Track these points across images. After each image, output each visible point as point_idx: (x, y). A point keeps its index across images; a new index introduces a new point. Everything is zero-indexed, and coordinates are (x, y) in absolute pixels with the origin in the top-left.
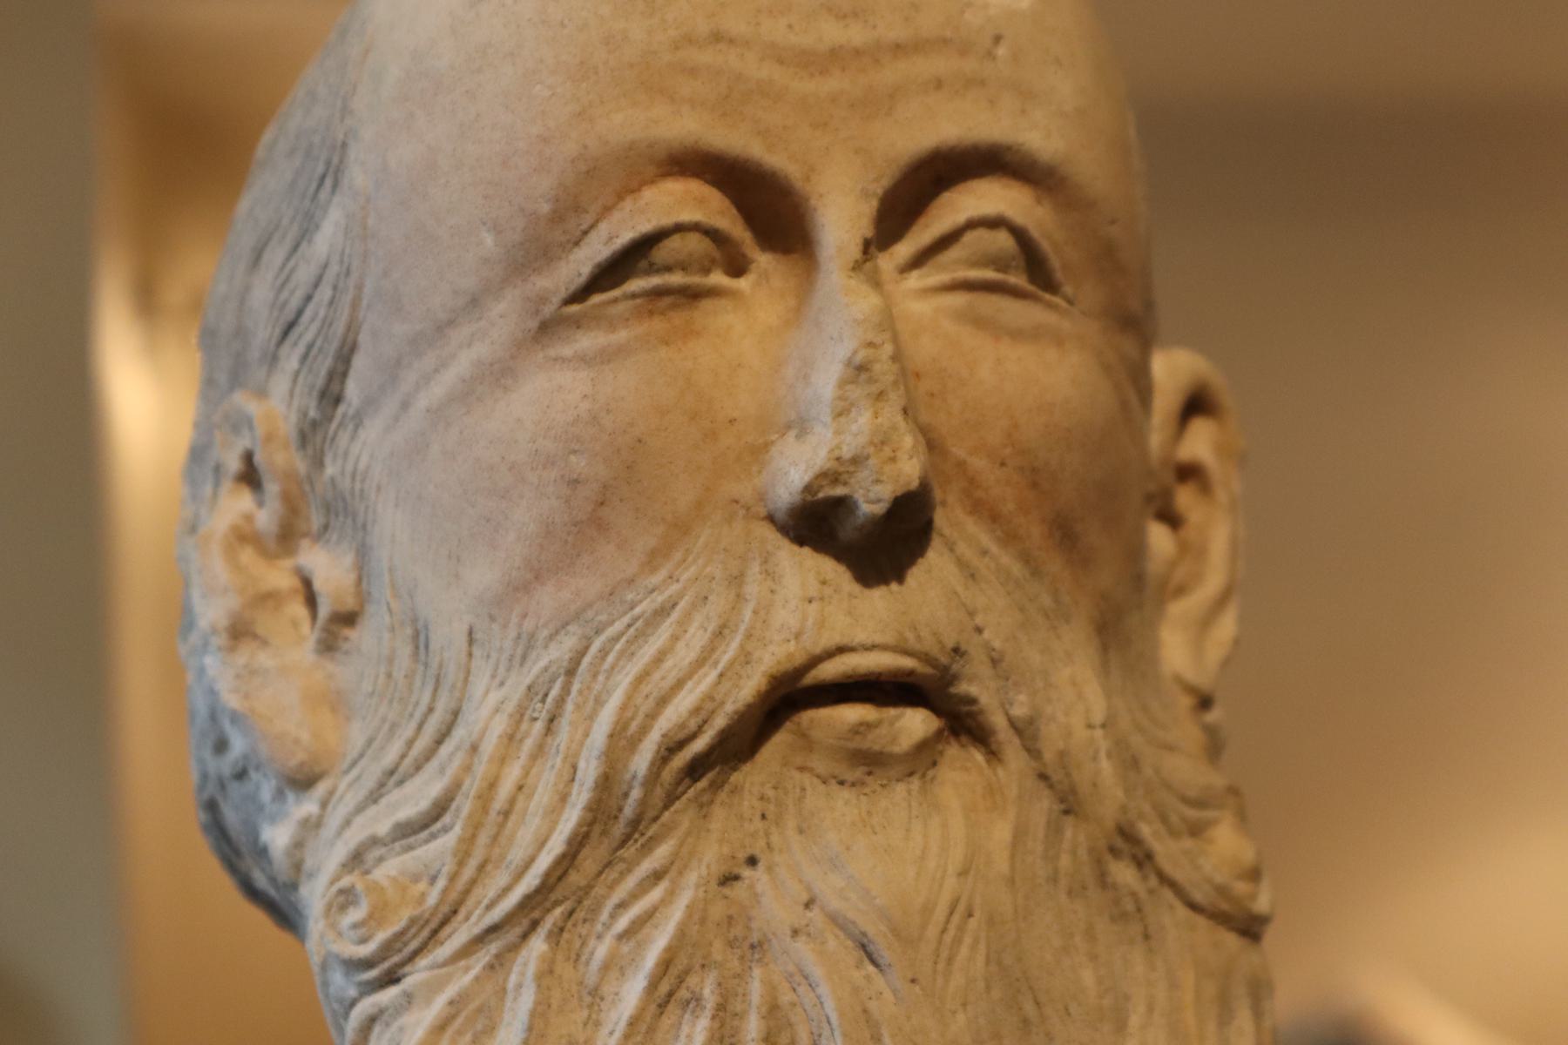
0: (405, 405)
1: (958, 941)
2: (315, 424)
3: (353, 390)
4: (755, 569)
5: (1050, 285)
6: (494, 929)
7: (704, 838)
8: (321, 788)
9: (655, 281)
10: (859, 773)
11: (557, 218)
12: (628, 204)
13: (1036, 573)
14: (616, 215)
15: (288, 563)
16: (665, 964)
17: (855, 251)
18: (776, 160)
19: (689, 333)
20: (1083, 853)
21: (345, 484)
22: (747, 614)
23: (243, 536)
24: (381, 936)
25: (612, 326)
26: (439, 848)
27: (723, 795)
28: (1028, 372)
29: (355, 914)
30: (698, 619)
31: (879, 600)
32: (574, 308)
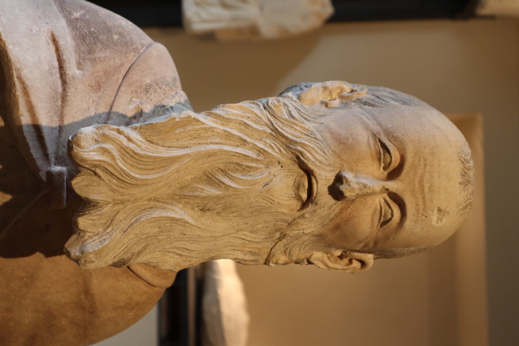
0: (363, 114)
1: (267, 201)
2: (361, 101)
3: (366, 107)
4: (332, 168)
5: (381, 226)
6: (272, 124)
7: (286, 158)
8: (298, 101)
9: (382, 153)
10: (296, 186)
11: (394, 137)
12: (396, 148)
13: (330, 221)
14: (394, 147)
15: (337, 97)
16: (265, 151)
17: (386, 187)
18: (403, 174)
19: (373, 159)
20: (281, 226)
21: (350, 106)
22: (324, 167)
23: (342, 90)
24: (272, 107)
25: (374, 146)
26: (286, 116)
27: (293, 162)
28: (365, 221)
29: (276, 103)
30: (323, 159)
31: (326, 190)
32: (378, 140)
